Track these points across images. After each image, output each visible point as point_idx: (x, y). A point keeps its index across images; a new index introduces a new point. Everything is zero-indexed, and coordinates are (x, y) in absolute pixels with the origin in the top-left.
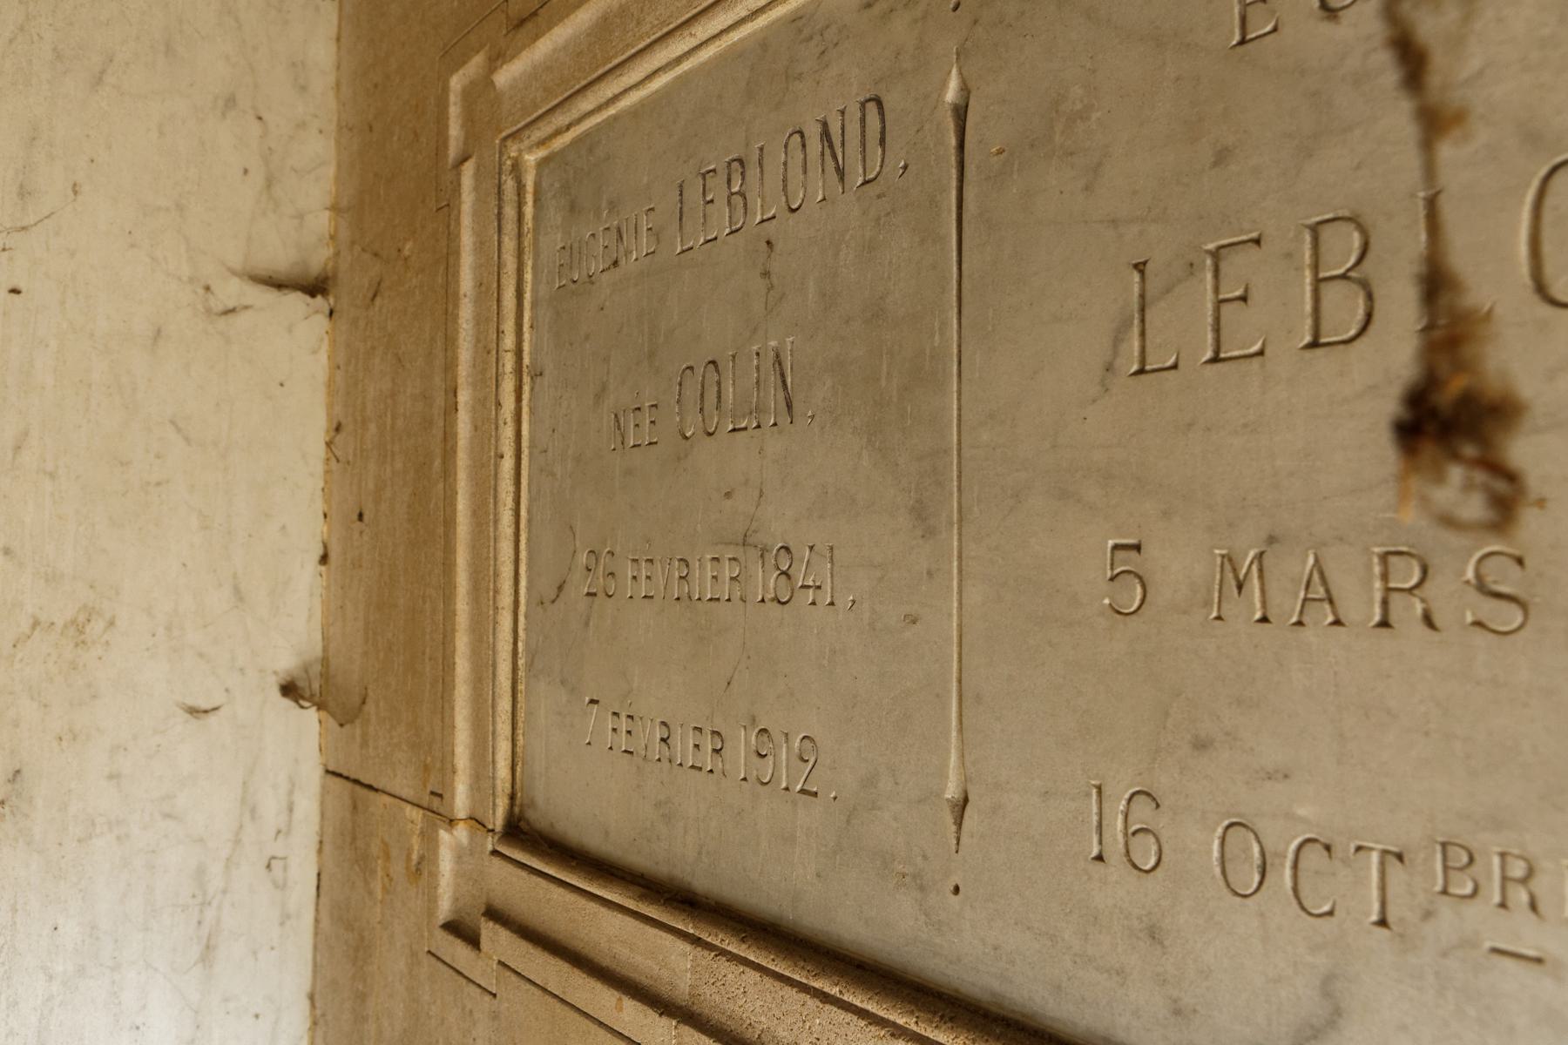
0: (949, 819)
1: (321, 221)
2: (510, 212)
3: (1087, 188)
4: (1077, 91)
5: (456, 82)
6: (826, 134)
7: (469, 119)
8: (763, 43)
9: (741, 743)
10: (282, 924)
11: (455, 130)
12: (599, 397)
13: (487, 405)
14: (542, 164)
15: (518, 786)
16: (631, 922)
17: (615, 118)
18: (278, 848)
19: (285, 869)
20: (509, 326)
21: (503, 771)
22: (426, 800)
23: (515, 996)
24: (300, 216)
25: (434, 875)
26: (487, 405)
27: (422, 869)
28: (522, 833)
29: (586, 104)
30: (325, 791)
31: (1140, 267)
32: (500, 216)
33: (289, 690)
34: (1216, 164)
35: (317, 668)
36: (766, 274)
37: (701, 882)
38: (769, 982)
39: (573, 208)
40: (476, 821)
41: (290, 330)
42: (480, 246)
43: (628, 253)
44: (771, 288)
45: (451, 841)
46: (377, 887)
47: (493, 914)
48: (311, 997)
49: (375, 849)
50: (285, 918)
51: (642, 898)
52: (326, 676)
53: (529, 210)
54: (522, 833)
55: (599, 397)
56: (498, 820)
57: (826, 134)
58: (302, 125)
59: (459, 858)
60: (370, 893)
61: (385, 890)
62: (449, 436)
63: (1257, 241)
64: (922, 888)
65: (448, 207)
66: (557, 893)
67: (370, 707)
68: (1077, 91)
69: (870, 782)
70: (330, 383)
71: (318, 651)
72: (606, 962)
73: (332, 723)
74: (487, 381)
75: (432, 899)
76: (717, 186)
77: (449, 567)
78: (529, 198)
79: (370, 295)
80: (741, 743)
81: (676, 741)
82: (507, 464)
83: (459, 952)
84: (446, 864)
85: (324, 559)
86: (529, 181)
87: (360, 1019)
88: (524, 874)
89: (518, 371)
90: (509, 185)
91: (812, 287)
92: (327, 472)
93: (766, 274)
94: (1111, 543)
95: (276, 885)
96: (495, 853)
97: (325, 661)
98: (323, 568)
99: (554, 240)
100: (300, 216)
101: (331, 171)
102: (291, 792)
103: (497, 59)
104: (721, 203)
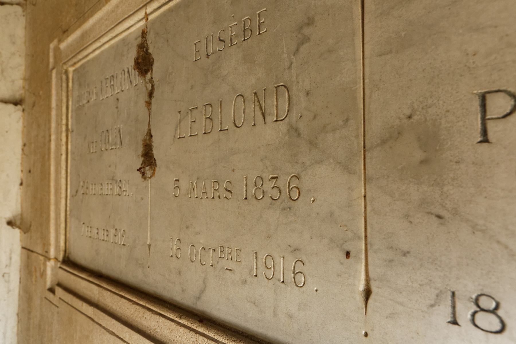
0: (148, 248)
1: (20, 83)
2: (64, 85)
3: (172, 92)
4: (170, 68)
5: (52, 46)
6: (128, 72)
7: (55, 58)
8: (117, 45)
9: (112, 231)
10: (8, 293)
11: (51, 60)
12: (85, 138)
13: (59, 139)
14: (74, 71)
15: (67, 248)
16: (87, 283)
17: (88, 61)
18: (6, 270)
19: (9, 276)
20: (64, 117)
21: (62, 244)
22: (44, 254)
23: (63, 307)
24: (13, 81)
25: (46, 275)
26: (59, 139)
27: (43, 274)
28: (69, 262)
29: (80, 57)
30: (22, 253)
31: (179, 112)
32: (61, 86)
33: (10, 223)
34: (191, 89)
35: (19, 217)
36: (117, 108)
37: (105, 271)
38: (112, 294)
39: (80, 85)
40: (56, 259)
41: (10, 115)
42: (57, 93)
43: (91, 99)
44: (118, 111)
45: (50, 264)
46: (33, 280)
47: (59, 285)
48: (18, 315)
49: (33, 269)
50: (9, 291)
51: (90, 276)
52: (22, 219)
53: (70, 84)
54: (69, 262)
55: (85, 138)
56: (61, 258)
57: (128, 72)
58: (13, 54)
59: (52, 270)
60: (32, 282)
61: (36, 281)
62: (49, 149)
63: (197, 108)
64: (143, 267)
65: (49, 82)
66: (72, 277)
67: (32, 228)
68: (170, 68)
69: (134, 241)
70: (23, 132)
71: (20, 212)
72: (81, 294)
73: (23, 233)
74: (59, 133)
75: (45, 282)
76: (108, 81)
77: (49, 186)
78: (71, 81)
79: (130, 83)
80: (112, 231)
81: (100, 233)
82: (64, 157)
83: (50, 296)
84: (49, 272)
85: (21, 184)
86: (70, 76)
87: (29, 319)
88: (65, 272)
89: (67, 130)
90: (64, 77)
91: (125, 111)
92: (22, 158)
93: (117, 108)
94: (174, 179)
95: (6, 281)
96: (60, 267)
97: (22, 214)
98: (21, 187)
99: (76, 93)
100: (13, 81)
101: (23, 68)
102: (11, 254)
103: (60, 41)
104: (109, 87)
